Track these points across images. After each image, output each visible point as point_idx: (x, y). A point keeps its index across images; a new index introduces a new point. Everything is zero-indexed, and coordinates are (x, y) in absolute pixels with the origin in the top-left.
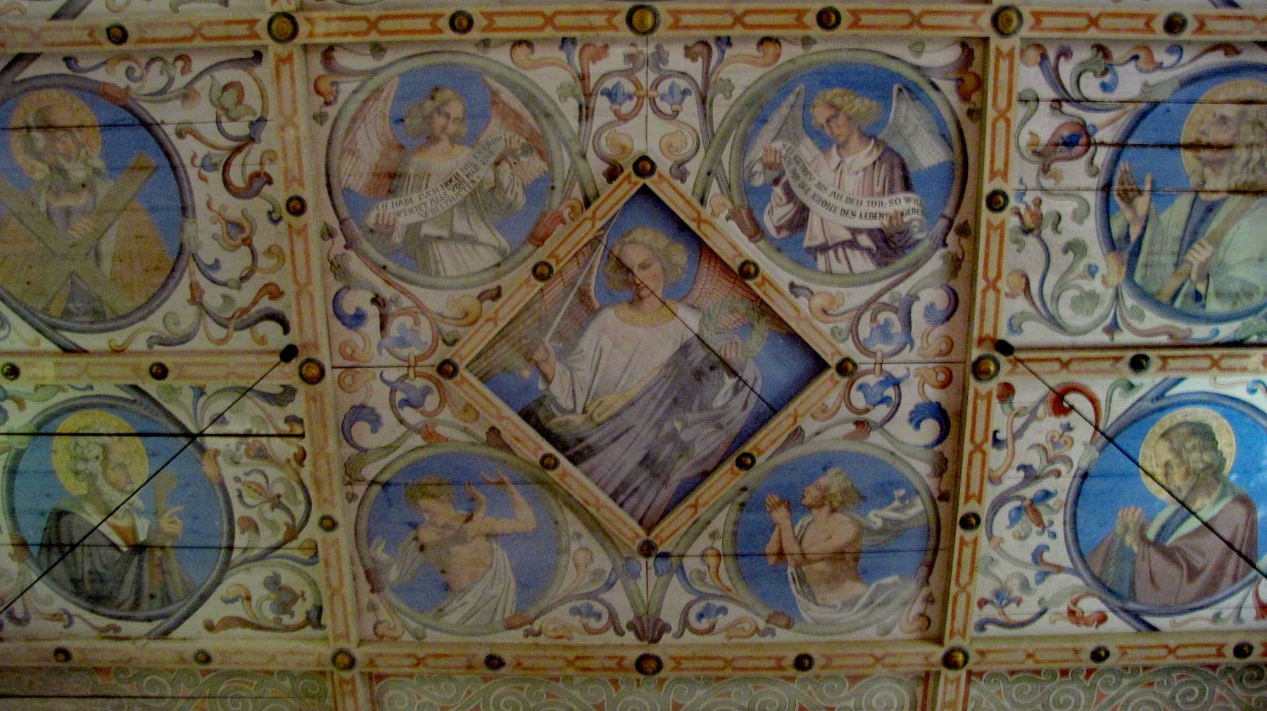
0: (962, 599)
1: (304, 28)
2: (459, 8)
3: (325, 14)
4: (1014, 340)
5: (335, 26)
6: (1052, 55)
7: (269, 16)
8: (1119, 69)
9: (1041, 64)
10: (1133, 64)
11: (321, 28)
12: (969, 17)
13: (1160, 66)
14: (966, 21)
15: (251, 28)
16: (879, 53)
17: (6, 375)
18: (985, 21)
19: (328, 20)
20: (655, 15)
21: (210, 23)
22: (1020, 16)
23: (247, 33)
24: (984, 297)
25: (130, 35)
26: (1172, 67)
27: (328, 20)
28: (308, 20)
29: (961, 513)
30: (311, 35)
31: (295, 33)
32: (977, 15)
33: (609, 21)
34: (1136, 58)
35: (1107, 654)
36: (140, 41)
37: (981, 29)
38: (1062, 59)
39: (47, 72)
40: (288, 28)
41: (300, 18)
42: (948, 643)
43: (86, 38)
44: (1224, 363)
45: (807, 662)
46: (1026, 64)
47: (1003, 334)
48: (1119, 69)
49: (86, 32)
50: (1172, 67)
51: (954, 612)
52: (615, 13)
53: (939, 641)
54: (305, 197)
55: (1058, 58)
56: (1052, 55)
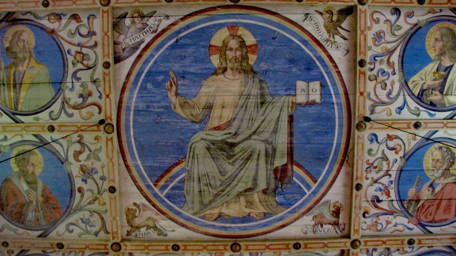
0: (360, 162)
1: (123, 248)
2: (168, 4)
3: (130, 243)
4: (372, 117)
5: (133, 247)
6: (370, 250)
7: (112, 243)
8: (393, 254)
9: (367, 254)
10: (397, 252)
11: (129, 248)
12: (343, 243)
13: (406, 252)
14: (342, 245)
15: (105, 247)
16: (314, 253)
17: (3, 244)
18: (348, 244)
19: (131, 245)
20: (240, 246)
21: (92, 244)
22: (360, 242)
23: (104, 248)
24: (359, 100)
25: (64, 244)
26: (411, 252)
27: (131, 245)
28: (125, 245)
29: (358, 59)
30: (125, 250)
31: (120, 249)
32: (345, 243)
33: (224, 248)
34: (398, 250)
35: (414, 241)
36: (68, 248)
37: (347, 247)
38: (374, 251)
39: (35, 253)
40: (118, 248)
41: (122, 244)
42: (353, 238)
43: (50, 246)
44: (449, 125)
45: (298, 246)
46: (362, 254)
47: (368, 114)
48: (393, 254)
49: (50, 245)
50: (411, 252)
51: (359, 87)
52: (226, 245)
53: (348, 237)
54: (116, 187)
55: (372, 251)
56: (370, 250)
